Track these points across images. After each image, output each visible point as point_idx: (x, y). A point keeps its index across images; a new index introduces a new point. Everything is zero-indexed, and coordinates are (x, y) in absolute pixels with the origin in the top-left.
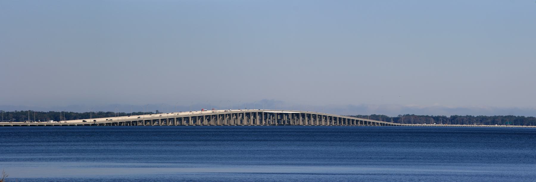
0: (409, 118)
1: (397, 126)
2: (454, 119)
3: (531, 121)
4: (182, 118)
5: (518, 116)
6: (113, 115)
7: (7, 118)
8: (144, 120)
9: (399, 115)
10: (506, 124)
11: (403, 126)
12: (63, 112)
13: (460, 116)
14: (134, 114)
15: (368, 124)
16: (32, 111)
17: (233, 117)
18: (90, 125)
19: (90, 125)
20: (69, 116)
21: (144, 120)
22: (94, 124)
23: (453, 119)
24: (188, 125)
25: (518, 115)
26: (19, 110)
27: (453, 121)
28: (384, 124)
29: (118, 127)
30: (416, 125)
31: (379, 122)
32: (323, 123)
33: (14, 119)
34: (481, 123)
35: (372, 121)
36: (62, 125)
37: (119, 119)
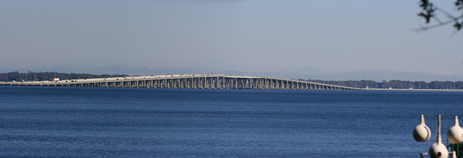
0: (364, 83)
1: (356, 91)
2: (432, 85)
3: (458, 85)
4: (158, 80)
5: (415, 82)
6: (109, 76)
7: (31, 78)
8: (107, 82)
9: (383, 81)
10: (442, 89)
11: (362, 90)
12: (84, 74)
13: (51, 73)
14: (102, 76)
15: (335, 88)
16: (56, 72)
17: (261, 81)
18: (54, 86)
19: (61, 86)
20: (50, 76)
21: (107, 82)
22: (59, 84)
23: (431, 85)
24: (197, 88)
25: (415, 81)
26: (44, 71)
27: (431, 86)
28: (343, 88)
29: (95, 88)
30: (439, 90)
31: (339, 87)
32: (283, 87)
33: (37, 79)
34: (456, 88)
35: (331, 86)
36: (35, 85)
37: (82, 81)
